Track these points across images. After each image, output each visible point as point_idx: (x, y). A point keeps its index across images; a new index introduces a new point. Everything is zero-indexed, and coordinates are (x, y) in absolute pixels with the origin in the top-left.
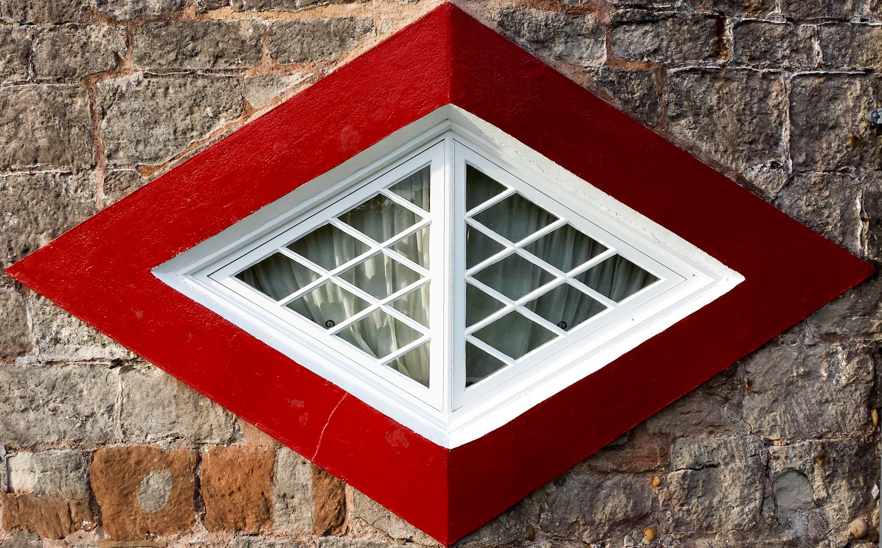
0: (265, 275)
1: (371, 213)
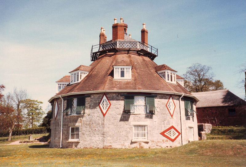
0: (167, 134)
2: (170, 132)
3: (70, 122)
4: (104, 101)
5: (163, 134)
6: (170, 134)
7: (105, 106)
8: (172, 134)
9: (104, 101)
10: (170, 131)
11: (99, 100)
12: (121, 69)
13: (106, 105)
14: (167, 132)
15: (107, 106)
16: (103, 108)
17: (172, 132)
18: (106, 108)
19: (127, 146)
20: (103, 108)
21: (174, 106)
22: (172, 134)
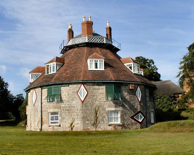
0: (136, 117)
1: (138, 116)
2: (138, 116)
3: (50, 109)
4: (84, 96)
5: (132, 118)
6: (138, 117)
7: (82, 94)
8: (139, 117)
9: (84, 96)
10: (138, 115)
11: (77, 89)
12: (95, 61)
13: (81, 93)
14: (136, 116)
15: (80, 91)
16: (81, 96)
17: (139, 116)
18: (81, 90)
19: (103, 128)
20: (81, 96)
21: (87, 93)
22: (139, 117)
